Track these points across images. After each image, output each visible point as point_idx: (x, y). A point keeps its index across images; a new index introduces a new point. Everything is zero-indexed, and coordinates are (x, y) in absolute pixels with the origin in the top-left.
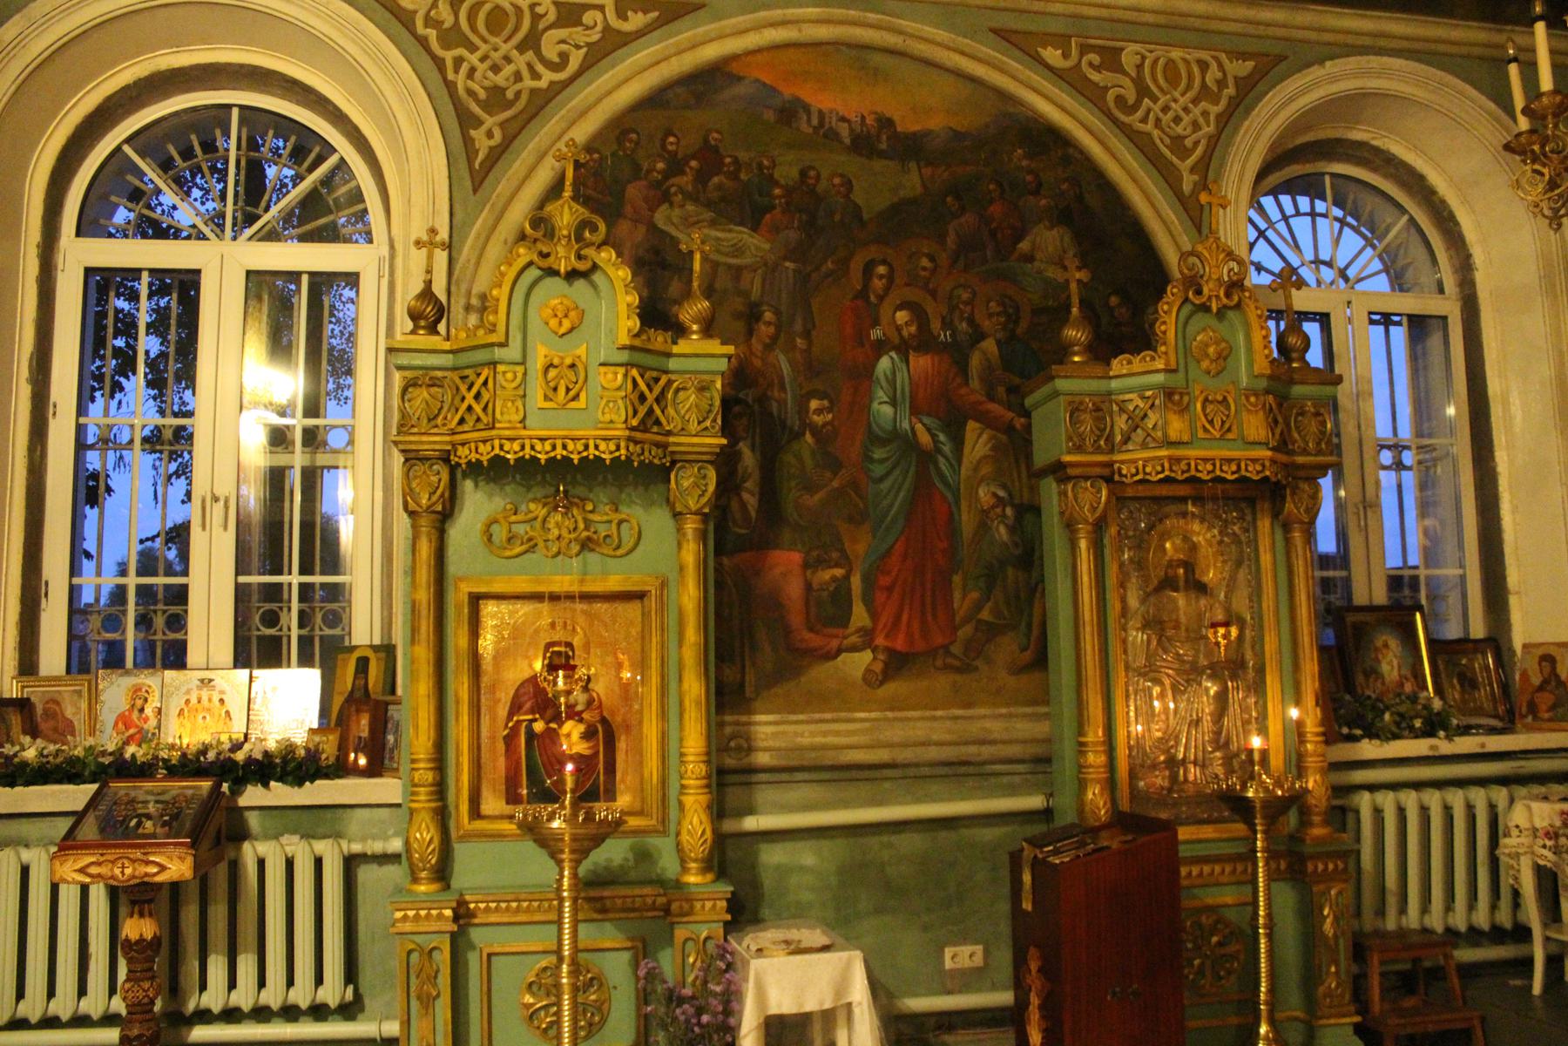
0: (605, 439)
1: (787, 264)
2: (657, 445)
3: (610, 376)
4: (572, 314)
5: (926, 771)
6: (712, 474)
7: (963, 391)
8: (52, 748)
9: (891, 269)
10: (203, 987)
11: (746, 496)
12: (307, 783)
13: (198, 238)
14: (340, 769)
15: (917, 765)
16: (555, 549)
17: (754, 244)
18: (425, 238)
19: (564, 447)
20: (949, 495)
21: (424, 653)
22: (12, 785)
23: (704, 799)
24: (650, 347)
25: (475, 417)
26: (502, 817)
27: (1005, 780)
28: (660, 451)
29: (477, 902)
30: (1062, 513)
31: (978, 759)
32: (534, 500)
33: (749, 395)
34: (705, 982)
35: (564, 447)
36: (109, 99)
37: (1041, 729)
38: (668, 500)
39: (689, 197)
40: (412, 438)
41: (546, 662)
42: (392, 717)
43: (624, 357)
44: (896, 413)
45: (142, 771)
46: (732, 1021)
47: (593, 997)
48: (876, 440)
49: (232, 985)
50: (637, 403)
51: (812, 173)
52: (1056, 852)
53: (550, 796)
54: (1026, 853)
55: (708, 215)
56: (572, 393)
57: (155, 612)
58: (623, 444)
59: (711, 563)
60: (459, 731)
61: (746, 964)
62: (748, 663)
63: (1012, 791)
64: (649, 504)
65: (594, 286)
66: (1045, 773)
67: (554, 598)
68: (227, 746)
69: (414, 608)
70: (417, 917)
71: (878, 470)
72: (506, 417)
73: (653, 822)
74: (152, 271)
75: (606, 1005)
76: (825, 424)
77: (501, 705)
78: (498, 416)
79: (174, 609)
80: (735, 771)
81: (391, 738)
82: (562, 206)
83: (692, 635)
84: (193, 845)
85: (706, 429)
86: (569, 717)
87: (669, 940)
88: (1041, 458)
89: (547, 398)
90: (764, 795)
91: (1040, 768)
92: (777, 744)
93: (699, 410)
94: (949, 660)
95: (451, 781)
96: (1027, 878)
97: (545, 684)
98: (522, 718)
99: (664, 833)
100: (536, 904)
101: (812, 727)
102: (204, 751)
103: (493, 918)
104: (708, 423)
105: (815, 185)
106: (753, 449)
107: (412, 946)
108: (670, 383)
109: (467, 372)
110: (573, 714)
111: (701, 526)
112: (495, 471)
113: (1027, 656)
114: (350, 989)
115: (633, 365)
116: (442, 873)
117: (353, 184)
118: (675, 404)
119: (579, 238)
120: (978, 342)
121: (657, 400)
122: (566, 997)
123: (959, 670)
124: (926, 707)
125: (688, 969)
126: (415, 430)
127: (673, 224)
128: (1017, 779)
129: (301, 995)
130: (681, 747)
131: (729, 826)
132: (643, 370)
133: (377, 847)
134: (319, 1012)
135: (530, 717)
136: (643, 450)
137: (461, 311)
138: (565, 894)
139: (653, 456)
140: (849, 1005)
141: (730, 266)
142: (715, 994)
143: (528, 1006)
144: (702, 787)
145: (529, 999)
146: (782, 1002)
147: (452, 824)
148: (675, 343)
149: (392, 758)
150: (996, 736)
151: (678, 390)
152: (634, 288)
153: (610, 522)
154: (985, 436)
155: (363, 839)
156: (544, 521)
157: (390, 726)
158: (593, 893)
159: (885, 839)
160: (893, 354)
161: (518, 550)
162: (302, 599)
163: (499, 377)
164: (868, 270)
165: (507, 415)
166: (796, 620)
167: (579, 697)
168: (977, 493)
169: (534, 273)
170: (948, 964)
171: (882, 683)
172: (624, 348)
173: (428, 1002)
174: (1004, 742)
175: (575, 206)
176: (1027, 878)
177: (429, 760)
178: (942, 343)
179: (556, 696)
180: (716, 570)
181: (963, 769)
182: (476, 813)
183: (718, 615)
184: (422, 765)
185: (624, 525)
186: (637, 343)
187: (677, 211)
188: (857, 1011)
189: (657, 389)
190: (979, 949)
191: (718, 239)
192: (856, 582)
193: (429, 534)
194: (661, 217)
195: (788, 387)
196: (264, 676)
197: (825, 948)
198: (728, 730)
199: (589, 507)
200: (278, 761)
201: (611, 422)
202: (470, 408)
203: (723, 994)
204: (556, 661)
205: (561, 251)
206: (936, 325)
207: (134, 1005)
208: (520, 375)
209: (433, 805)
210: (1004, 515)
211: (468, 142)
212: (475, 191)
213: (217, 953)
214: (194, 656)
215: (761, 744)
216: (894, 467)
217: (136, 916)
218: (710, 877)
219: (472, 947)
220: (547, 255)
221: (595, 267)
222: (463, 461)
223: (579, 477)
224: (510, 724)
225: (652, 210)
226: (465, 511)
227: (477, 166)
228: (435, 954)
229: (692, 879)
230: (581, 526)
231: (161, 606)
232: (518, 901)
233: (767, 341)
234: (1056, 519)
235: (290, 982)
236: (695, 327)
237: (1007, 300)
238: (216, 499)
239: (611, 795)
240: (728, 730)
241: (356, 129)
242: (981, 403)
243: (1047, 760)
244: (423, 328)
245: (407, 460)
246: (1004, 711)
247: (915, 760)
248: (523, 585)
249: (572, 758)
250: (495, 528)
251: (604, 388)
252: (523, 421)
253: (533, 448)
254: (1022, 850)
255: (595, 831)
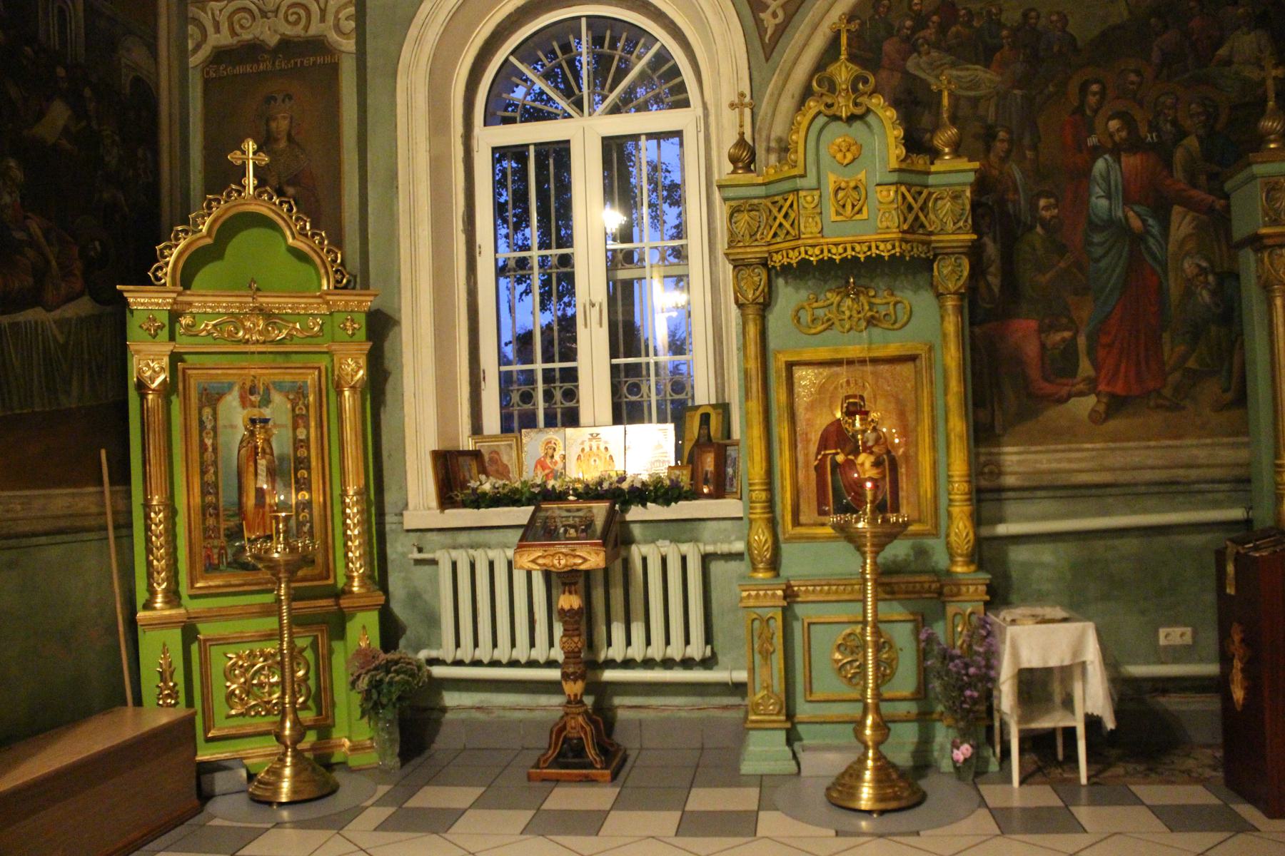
0: (884, 241)
1: (1016, 92)
2: (923, 243)
3: (885, 193)
4: (853, 148)
5: (1143, 489)
6: (966, 263)
7: (1168, 182)
8: (500, 483)
9: (1104, 88)
10: (609, 644)
11: (990, 278)
12: (673, 504)
13: (565, 117)
14: (694, 495)
15: (1136, 485)
16: (847, 326)
17: (985, 77)
18: (737, 101)
19: (853, 249)
20: (1158, 269)
21: (755, 406)
22: (478, 507)
23: (967, 509)
24: (914, 168)
25: (785, 231)
26: (815, 525)
27: (1210, 496)
28: (925, 247)
29: (799, 586)
30: (1259, 277)
31: (1185, 480)
32: (830, 290)
33: (989, 199)
34: (970, 646)
35: (853, 249)
36: (499, 25)
37: (1243, 455)
38: (932, 285)
39: (937, 46)
40: (739, 250)
41: (844, 410)
42: (730, 455)
43: (894, 177)
44: (1111, 204)
45: (560, 496)
46: (992, 673)
47: (885, 656)
48: (1093, 227)
49: (629, 643)
50: (906, 211)
51: (1033, 14)
52: (1256, 549)
53: (853, 508)
54: (1229, 550)
55: (948, 59)
56: (856, 209)
57: (554, 388)
58: (897, 244)
59: (967, 332)
60: (783, 462)
61: (1003, 631)
62: (996, 407)
63: (1216, 505)
64: (916, 289)
65: (869, 126)
66: (1246, 491)
67: (850, 362)
68: (615, 478)
69: (746, 374)
70: (757, 596)
71: (1099, 251)
72: (809, 230)
73: (928, 527)
74: (535, 145)
75: (894, 662)
76: (1053, 217)
77: (812, 443)
78: (802, 229)
79: (568, 385)
80: (991, 490)
81: (730, 471)
82: (840, 67)
83: (955, 385)
84: (604, 544)
85: (960, 228)
86: (864, 451)
87: (942, 615)
88: (1240, 230)
89: (838, 213)
90: (1011, 508)
91: (1241, 486)
92: (1021, 469)
93: (954, 215)
94: (1161, 401)
95: (778, 499)
96: (1230, 568)
97: (847, 426)
98: (828, 452)
99: (936, 535)
100: (842, 588)
101: (1050, 456)
102: (600, 483)
103: (811, 598)
104: (961, 224)
105: (1036, 24)
106: (995, 241)
107: (755, 616)
108: (930, 194)
109: (776, 198)
110: (868, 450)
111: (958, 303)
112: (802, 271)
113: (1229, 396)
114: (709, 648)
115: (902, 184)
116: (774, 564)
117: (671, 63)
118: (935, 211)
119: (855, 89)
120: (1181, 140)
121: (922, 209)
122: (870, 650)
123: (1168, 409)
124: (1140, 439)
125: (957, 636)
126: (741, 244)
127: (921, 68)
128: (1220, 496)
129: (676, 652)
130: (949, 470)
131: (985, 531)
132: (909, 186)
133: (724, 548)
134: (687, 663)
135: (833, 451)
136: (912, 248)
137: (763, 152)
138: (868, 576)
139: (919, 251)
140: (1084, 663)
141: (969, 99)
142: (977, 653)
143: (837, 661)
144: (966, 500)
145: (838, 656)
146: (1031, 659)
147: (780, 530)
148: (932, 163)
149: (732, 485)
150: (1200, 461)
151: (936, 200)
152: (900, 124)
153: (888, 303)
154: (1188, 218)
155: (715, 543)
156: (839, 305)
157: (729, 462)
158: (885, 580)
159: (1110, 542)
160: (1107, 156)
161: (820, 328)
162: (545, 381)
163: (801, 200)
164: (1084, 88)
165: (809, 228)
166: (1034, 373)
167: (870, 435)
168: (1182, 264)
169: (821, 120)
170: (1162, 641)
171: (1106, 419)
172: (894, 171)
173: (766, 655)
174: (1208, 466)
175: (850, 65)
176: (1230, 568)
177: (762, 484)
178: (1150, 143)
179: (854, 436)
180: (971, 337)
181: (1174, 488)
182: (796, 522)
183: (973, 374)
184: (757, 488)
185: (899, 306)
186: (904, 166)
187: (924, 58)
188: (1090, 668)
189: (921, 201)
190: (1188, 630)
191: (959, 77)
192: (1082, 341)
193: (755, 320)
194: (910, 65)
195: (1020, 190)
196: (633, 429)
197: (1065, 620)
198: (982, 459)
199: (872, 293)
200: (651, 488)
201: (888, 228)
202: (781, 225)
203: (986, 653)
204: (852, 409)
205: (842, 101)
206: (1143, 130)
207: (569, 652)
208: (816, 198)
209: (766, 516)
210: (1206, 283)
211: (759, 23)
212: (767, 60)
213: (617, 621)
214: (584, 416)
215: (1008, 470)
216: (1110, 249)
217: (567, 593)
218: (973, 568)
219: (796, 618)
220: (832, 105)
221: (868, 111)
222: (778, 265)
223: (886, 270)
224: (819, 457)
225: (905, 59)
226: (779, 300)
227: (767, 41)
228: (772, 622)
229: (959, 569)
230: (867, 307)
231: (558, 384)
232: (829, 585)
233: (1002, 154)
234: (1254, 281)
235: (668, 642)
236: (947, 150)
237: (1207, 102)
238: (593, 305)
239: (896, 509)
240: (982, 459)
241: (672, 22)
242: (1185, 190)
243: (1248, 481)
244: (741, 168)
245: (735, 267)
246: (1209, 441)
247: (1133, 481)
248: (824, 354)
249: (871, 479)
250: (802, 313)
251: (880, 202)
252: (821, 232)
253: (829, 251)
254: (1226, 548)
255: (889, 531)
